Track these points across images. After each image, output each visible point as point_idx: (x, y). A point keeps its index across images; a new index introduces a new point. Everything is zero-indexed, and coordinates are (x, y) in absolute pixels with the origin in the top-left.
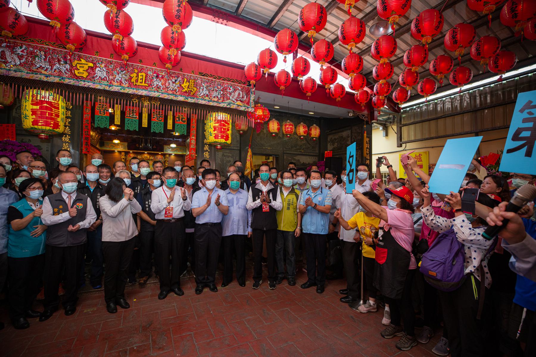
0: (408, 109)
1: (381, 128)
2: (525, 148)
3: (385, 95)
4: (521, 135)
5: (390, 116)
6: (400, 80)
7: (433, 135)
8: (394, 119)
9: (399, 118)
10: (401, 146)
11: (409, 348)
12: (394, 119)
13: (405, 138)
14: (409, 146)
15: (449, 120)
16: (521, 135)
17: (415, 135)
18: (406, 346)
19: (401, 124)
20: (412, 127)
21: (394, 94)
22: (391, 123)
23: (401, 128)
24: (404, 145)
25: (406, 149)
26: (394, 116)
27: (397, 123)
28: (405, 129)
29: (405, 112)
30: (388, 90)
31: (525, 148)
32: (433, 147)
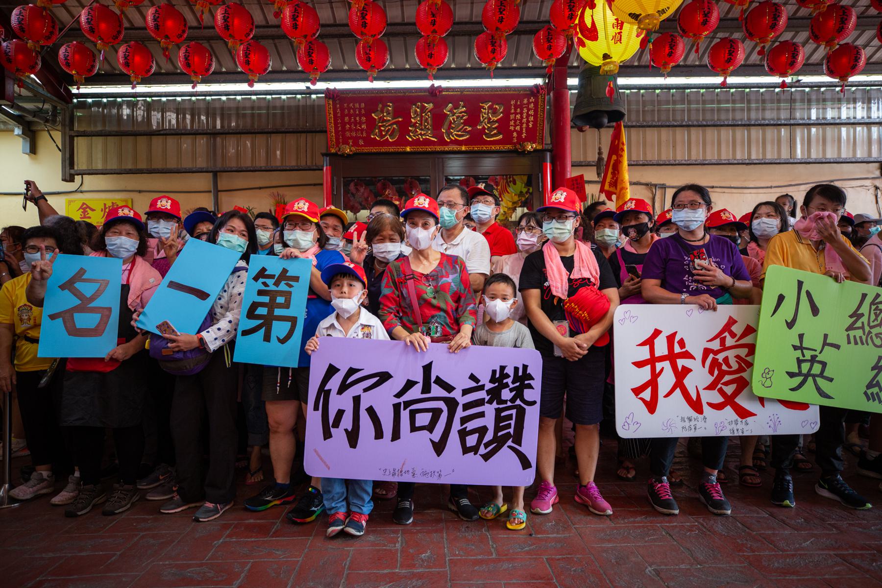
0: (90, 100)
1: (18, 131)
2: (263, 330)
3: (41, 42)
4: (257, 312)
5: (47, 106)
6: (83, 19)
7: (143, 166)
8: (55, 115)
9: (67, 115)
10: (72, 180)
11: (129, 506)
12: (55, 115)
13: (81, 163)
14: (90, 182)
15: (171, 141)
16: (257, 312)
17: (105, 160)
18: (123, 503)
19: (72, 129)
20: (98, 142)
21: (62, 51)
22: (47, 121)
23: (72, 139)
24: (78, 179)
25: (84, 188)
26: (55, 108)
27: (63, 125)
28: (81, 144)
29: (83, 106)
30: (52, 33)
31: (263, 330)
32: (140, 192)
